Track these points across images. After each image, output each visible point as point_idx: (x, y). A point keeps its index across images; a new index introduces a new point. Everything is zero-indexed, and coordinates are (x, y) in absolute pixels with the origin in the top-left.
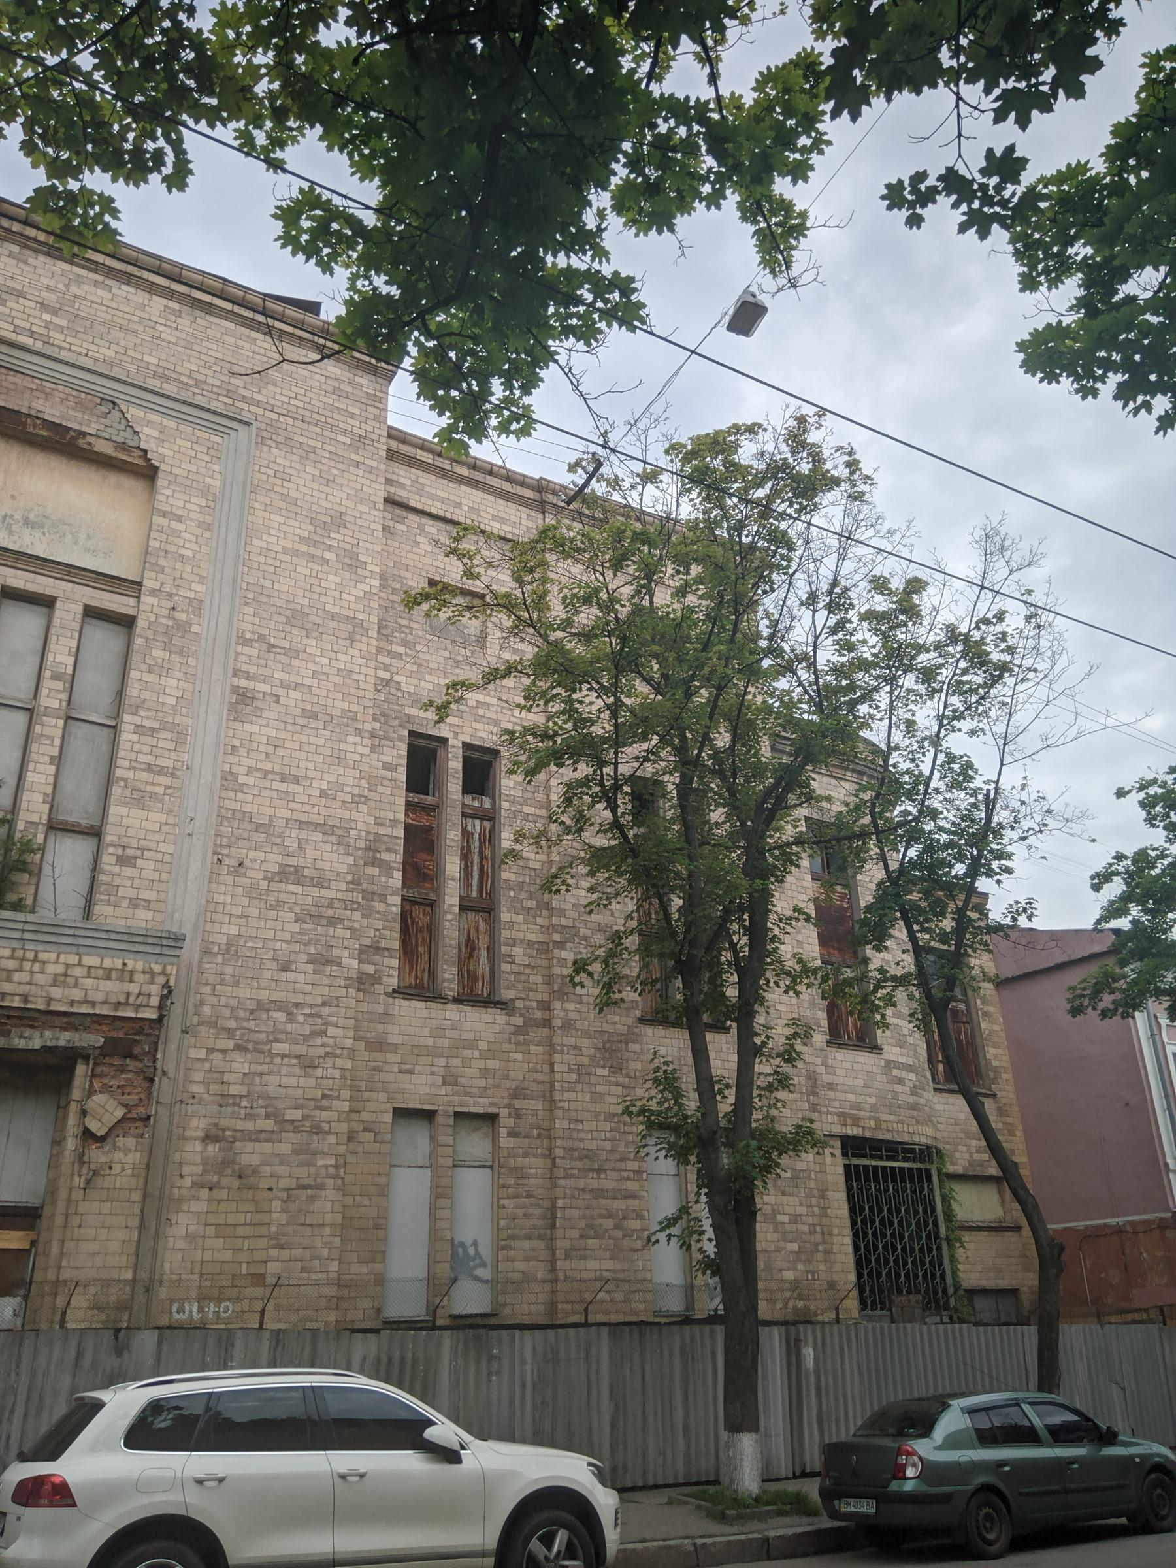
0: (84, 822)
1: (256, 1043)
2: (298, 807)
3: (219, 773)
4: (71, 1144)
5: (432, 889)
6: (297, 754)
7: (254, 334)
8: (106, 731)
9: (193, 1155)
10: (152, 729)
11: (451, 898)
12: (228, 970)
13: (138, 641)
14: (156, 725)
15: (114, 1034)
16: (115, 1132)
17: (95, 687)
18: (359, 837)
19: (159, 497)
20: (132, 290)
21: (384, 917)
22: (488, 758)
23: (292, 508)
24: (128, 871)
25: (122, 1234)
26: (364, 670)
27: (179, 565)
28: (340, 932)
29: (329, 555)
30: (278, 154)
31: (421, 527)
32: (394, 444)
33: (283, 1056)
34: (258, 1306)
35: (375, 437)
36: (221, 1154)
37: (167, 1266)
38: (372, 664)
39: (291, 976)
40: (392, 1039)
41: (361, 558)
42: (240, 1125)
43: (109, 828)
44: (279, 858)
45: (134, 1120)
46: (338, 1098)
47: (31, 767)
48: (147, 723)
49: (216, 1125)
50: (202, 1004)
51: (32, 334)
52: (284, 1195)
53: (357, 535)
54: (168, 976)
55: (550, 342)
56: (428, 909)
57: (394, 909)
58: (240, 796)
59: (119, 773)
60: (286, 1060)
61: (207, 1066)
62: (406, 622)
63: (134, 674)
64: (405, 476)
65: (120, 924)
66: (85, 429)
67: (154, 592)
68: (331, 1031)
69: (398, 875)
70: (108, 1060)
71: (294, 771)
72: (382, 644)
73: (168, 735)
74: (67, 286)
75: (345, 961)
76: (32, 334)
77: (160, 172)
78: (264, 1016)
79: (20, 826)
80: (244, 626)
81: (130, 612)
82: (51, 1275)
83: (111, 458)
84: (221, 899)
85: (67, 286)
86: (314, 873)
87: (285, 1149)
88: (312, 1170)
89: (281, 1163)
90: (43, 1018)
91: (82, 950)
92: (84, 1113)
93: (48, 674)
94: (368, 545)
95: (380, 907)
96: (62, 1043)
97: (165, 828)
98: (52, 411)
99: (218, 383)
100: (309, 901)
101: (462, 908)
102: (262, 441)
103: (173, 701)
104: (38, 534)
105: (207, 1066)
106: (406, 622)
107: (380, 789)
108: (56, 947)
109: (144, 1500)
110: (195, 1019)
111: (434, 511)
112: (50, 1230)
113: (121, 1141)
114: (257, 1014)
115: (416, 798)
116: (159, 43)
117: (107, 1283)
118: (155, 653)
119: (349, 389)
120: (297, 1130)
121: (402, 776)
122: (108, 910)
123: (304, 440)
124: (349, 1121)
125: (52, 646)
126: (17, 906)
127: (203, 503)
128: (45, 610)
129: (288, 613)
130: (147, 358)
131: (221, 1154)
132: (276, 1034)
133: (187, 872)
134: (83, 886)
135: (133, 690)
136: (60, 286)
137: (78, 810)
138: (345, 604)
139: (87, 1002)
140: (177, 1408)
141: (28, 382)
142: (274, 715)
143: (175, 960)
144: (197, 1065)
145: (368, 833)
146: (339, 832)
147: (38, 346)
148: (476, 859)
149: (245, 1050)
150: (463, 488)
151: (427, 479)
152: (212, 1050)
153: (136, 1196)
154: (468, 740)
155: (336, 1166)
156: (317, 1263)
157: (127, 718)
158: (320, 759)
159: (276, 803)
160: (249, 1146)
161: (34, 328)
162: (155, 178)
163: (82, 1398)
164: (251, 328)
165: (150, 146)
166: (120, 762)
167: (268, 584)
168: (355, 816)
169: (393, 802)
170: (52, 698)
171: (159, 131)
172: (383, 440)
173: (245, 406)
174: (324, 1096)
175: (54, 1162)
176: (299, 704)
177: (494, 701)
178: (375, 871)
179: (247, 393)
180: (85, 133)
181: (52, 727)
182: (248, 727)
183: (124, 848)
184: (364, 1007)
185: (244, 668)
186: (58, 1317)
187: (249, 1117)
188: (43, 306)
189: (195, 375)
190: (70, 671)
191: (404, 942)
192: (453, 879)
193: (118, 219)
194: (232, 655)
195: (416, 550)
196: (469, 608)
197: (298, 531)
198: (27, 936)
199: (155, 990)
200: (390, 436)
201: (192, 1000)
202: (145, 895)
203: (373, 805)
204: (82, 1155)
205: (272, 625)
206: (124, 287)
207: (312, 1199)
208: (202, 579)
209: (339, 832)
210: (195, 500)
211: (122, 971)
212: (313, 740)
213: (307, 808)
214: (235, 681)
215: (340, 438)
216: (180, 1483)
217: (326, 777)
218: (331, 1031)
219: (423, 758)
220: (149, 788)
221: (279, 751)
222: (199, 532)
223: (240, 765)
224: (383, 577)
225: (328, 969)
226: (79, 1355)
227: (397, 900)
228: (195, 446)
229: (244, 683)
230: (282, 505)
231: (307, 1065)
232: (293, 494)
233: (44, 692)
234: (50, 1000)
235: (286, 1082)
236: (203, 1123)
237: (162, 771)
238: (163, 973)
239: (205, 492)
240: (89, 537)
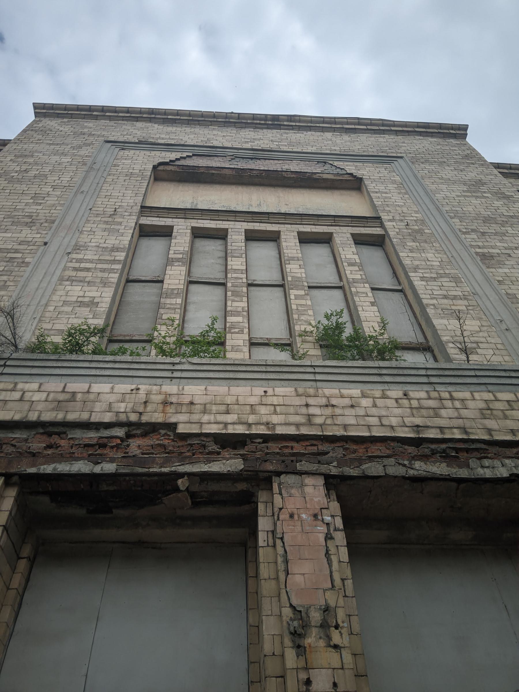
8: (397, 294)
234: (489, 431)
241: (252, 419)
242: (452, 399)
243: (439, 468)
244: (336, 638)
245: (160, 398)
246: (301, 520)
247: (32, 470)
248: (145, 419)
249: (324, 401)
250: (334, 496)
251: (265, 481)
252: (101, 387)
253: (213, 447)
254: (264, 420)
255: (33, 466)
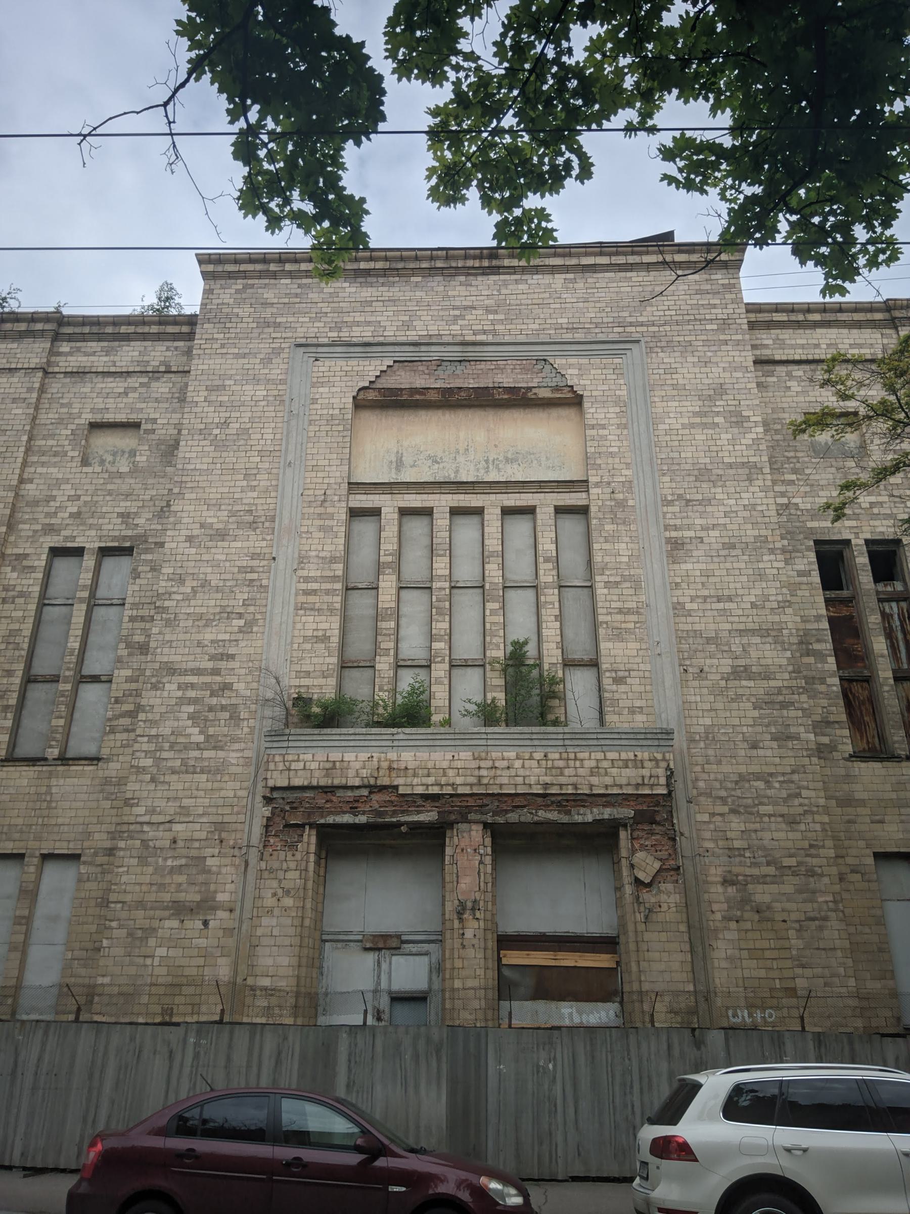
0: (586, 658)
1: (746, 807)
2: (736, 619)
3: (670, 605)
4: (628, 889)
5: (865, 667)
6: (726, 579)
7: (629, 274)
8: (586, 590)
9: (718, 896)
10: (617, 583)
11: (885, 672)
12: (711, 752)
13: (594, 522)
14: (618, 579)
15: (639, 807)
16: (659, 878)
17: (573, 560)
18: (791, 635)
19: (588, 416)
20: (540, 276)
21: (827, 696)
22: (892, 548)
23: (684, 393)
24: (622, 688)
25: (680, 957)
26: (765, 501)
27: (610, 460)
28: (793, 713)
29: (719, 420)
30: (650, 123)
31: (789, 374)
32: (753, 317)
33: (770, 816)
34: (795, 1013)
35: (736, 316)
36: (739, 895)
37: (717, 981)
38: (771, 494)
39: (761, 752)
40: (858, 796)
41: (744, 413)
42: (748, 871)
43: (603, 659)
44: (730, 662)
45: (668, 870)
46: (823, 847)
47: (544, 625)
48: (612, 579)
49: (730, 872)
50: (697, 780)
51: (485, 332)
52: (797, 926)
53: (737, 397)
54: (668, 761)
55: (901, 177)
56: (865, 685)
57: (835, 688)
58: (689, 619)
59: (601, 618)
60: (773, 819)
61: (712, 826)
62: (792, 454)
63: (596, 546)
64: (766, 338)
65: (625, 727)
66: (530, 385)
67: (597, 485)
68: (804, 793)
69: (832, 660)
70: (640, 827)
71: (726, 592)
72: (775, 477)
73: (628, 585)
74: (499, 291)
75: (803, 736)
76: (485, 332)
77: (571, 176)
78: (747, 785)
79: (546, 667)
80: (665, 491)
81: (584, 503)
82: (635, 987)
83: (550, 399)
84: (693, 699)
85: (499, 291)
86: (760, 669)
87: (788, 889)
88: (815, 905)
89: (788, 901)
90: (590, 800)
91: (605, 748)
92: (632, 866)
93: (541, 559)
94: (747, 402)
95: (822, 688)
96: (606, 817)
97: (641, 653)
98: (507, 380)
99: (611, 320)
100: (762, 691)
101: (896, 679)
102: (650, 350)
103: (626, 559)
104: (516, 466)
105: (712, 826)
106: (792, 454)
107: (799, 593)
108: (587, 749)
109: (747, 1161)
110: (695, 791)
111: (797, 357)
112: (627, 952)
113: (663, 886)
114: (741, 784)
115: (832, 594)
116: (552, 86)
117: (676, 994)
118: (607, 527)
119: (709, 287)
120: (795, 874)
121: (816, 578)
122: (615, 718)
123: (681, 339)
124: (837, 865)
125: (540, 540)
126: (556, 723)
127: (618, 410)
128: (530, 516)
129: (696, 473)
130: (560, 321)
131: (739, 895)
132: (760, 800)
133: (663, 682)
134: (595, 703)
135: (598, 558)
136: (495, 293)
137: (580, 652)
138: (739, 453)
139: (616, 785)
140: (753, 1091)
141: (489, 366)
142: (701, 553)
143: (670, 749)
144: (704, 827)
145: (798, 630)
146: (773, 633)
147: (490, 338)
148: (900, 636)
149: (739, 813)
150: (818, 331)
151: (786, 335)
152: (713, 815)
153: (683, 928)
154: (869, 536)
155: (835, 902)
156: (836, 980)
157: (598, 578)
158: (745, 579)
159: (718, 619)
160: (760, 888)
161: (486, 328)
162: (569, 182)
163: (684, 1080)
164: (626, 271)
165: (560, 160)
166: (600, 611)
167: (676, 455)
168: (784, 618)
169: (816, 602)
170: (547, 576)
171: (563, 147)
172: (743, 316)
173: (633, 329)
174: (811, 846)
175: (619, 903)
176: (719, 540)
177: (886, 499)
178: (811, 660)
179: (633, 319)
180: (517, 172)
181: (551, 596)
182: (683, 566)
183: (616, 671)
184: (828, 771)
185: (672, 522)
186: (647, 1019)
187: (754, 865)
188: (488, 310)
189: (594, 320)
190: (554, 554)
191: (850, 714)
192: (882, 656)
193: (551, 221)
194: (661, 515)
195: (788, 394)
196: (850, 425)
197: (690, 409)
198: (567, 742)
199: (661, 772)
200: (748, 311)
201: (689, 778)
202: (638, 703)
203: (797, 606)
204: (638, 898)
205: (686, 485)
206: (535, 277)
207: (821, 928)
208: (628, 465)
209: (773, 633)
210: (611, 410)
211: (635, 760)
212: (735, 565)
213: (743, 619)
214: (667, 534)
215: (708, 327)
216: (773, 1149)
217: (753, 592)
218: (804, 793)
219: (832, 561)
220: (623, 626)
221: (712, 579)
222: (619, 432)
223: (684, 595)
224: (765, 424)
225: (790, 744)
226: (669, 1047)
227: (836, 681)
228: (604, 371)
229: (674, 534)
230: (675, 392)
231: (792, 822)
232: (681, 382)
233: (541, 572)
234: (591, 786)
235: (777, 836)
236: (720, 871)
237: (629, 612)
238: (664, 759)
239: (618, 402)
240: (547, 459)
241: (443, 781)
242: (576, 759)
243: (553, 815)
244: (478, 915)
245: (385, 765)
246: (469, 845)
247: (322, 821)
248: (379, 783)
249: (490, 764)
250: (489, 833)
251: (451, 825)
252: (349, 756)
253: (420, 802)
254: (451, 782)
255: (322, 817)
